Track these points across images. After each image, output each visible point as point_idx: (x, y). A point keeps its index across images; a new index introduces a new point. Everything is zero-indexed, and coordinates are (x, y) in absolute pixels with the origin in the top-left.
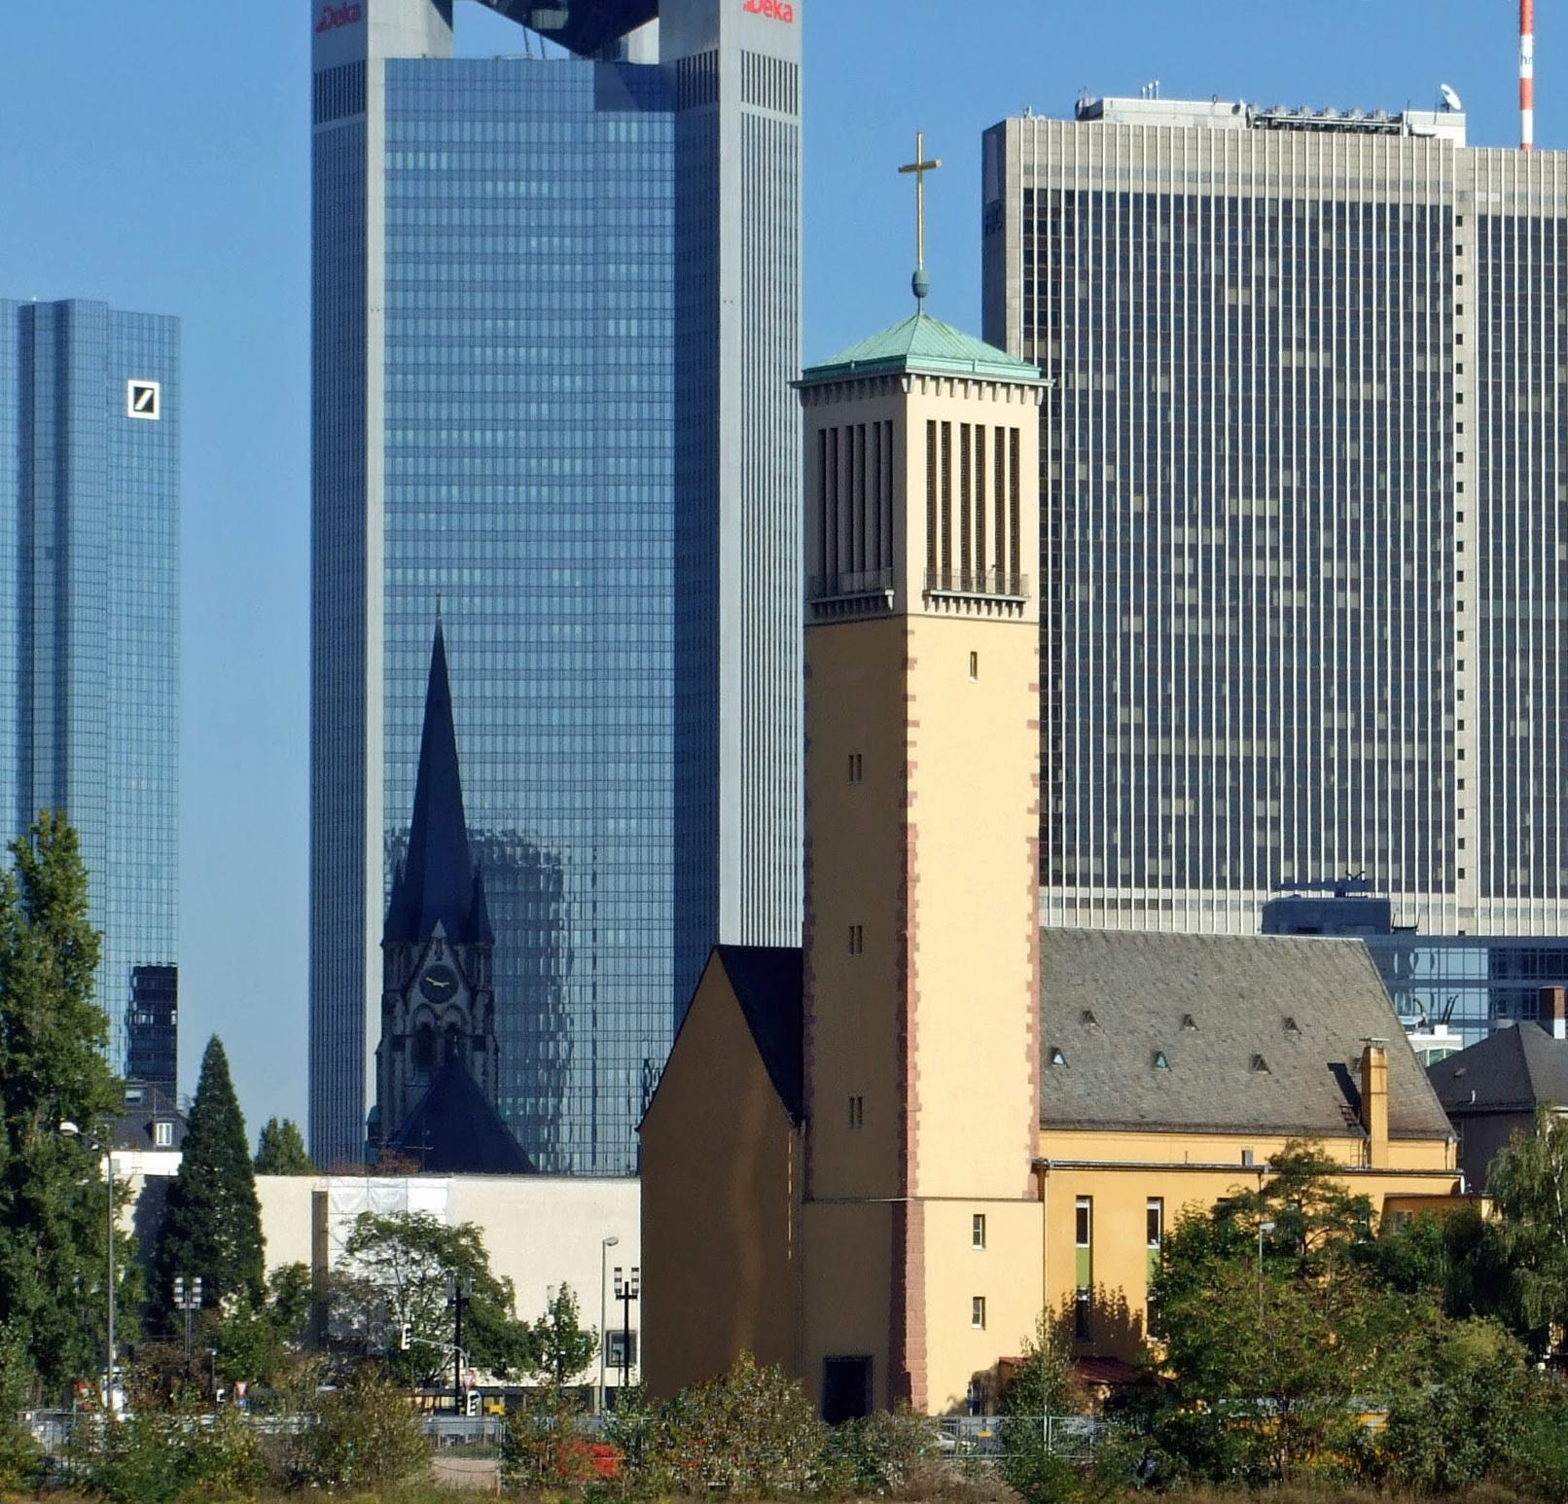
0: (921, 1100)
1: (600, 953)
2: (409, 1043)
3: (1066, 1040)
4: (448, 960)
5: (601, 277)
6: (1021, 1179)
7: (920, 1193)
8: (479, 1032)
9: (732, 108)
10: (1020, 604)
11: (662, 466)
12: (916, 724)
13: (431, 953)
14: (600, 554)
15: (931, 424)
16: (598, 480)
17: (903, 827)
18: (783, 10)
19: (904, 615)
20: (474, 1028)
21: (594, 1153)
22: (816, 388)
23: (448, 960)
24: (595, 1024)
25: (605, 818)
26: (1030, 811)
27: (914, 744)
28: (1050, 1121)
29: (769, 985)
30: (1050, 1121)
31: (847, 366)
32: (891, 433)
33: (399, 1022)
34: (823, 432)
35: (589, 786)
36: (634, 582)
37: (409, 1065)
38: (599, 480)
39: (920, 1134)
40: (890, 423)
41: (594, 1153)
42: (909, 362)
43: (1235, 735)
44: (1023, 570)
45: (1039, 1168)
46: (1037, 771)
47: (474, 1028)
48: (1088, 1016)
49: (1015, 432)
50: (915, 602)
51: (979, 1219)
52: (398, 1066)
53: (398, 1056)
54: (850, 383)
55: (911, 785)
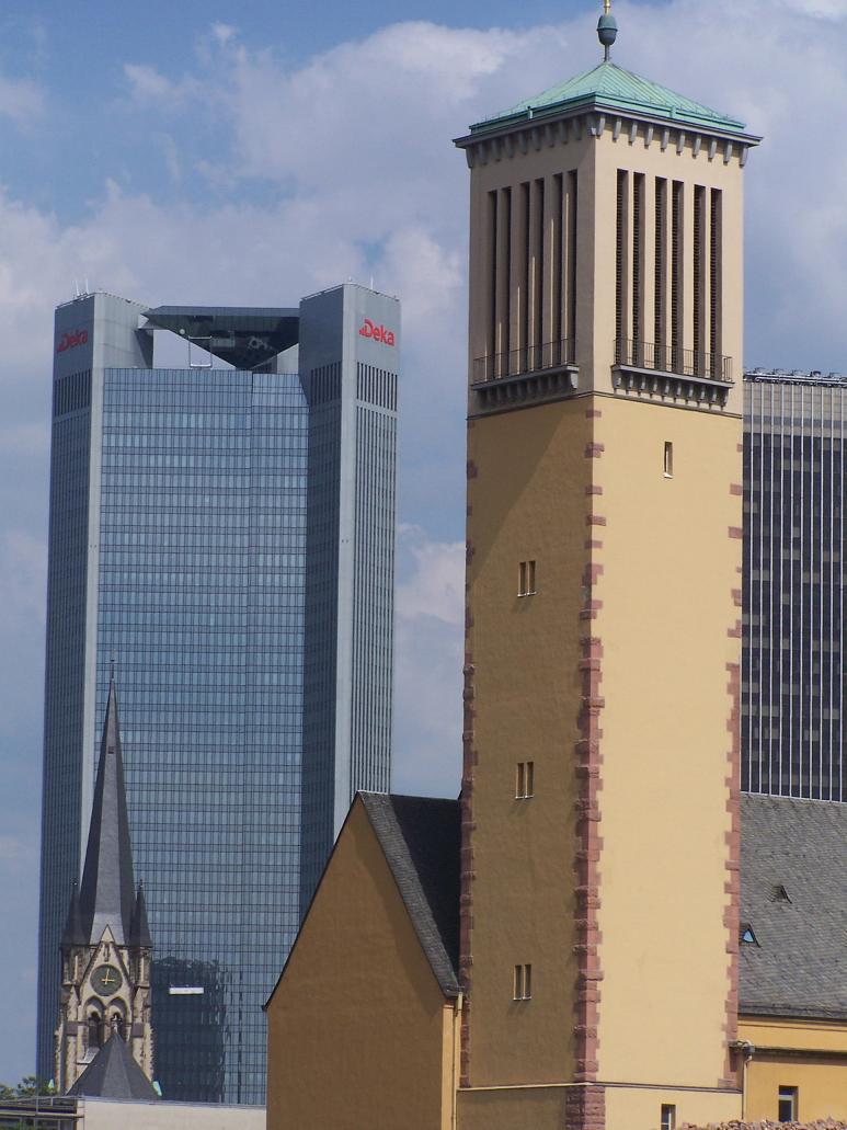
0: (602, 967)
1: (244, 1009)
2: (80, 1029)
3: (756, 916)
4: (114, 961)
5: (252, 642)
6: (715, 1065)
7: (600, 1076)
8: (139, 1020)
9: (349, 403)
10: (723, 392)
11: (295, 679)
12: (602, 522)
13: (100, 955)
14: (250, 722)
15: (622, 174)
16: (252, 550)
17: (587, 644)
18: (387, 337)
19: (591, 394)
20: (134, 1017)
21: (239, 1092)
22: (486, 144)
23: (114, 961)
24: (240, 1060)
25: (258, 514)
26: (731, 634)
27: (599, 545)
28: (748, 1012)
29: (436, 831)
30: (748, 1012)
31: (525, 114)
32: (573, 183)
33: (73, 1010)
34: (493, 195)
35: (240, 829)
36: (275, 682)
37: (80, 1046)
38: (253, 511)
39: (600, 1008)
40: (573, 174)
41: (239, 1092)
42: (597, 99)
43: (806, 771)
44: (725, 352)
45: (738, 1055)
46: (739, 586)
47: (134, 1017)
48: (781, 893)
49: (716, 194)
50: (602, 379)
51: (667, 1110)
52: (71, 1048)
53: (71, 1039)
54: (526, 133)
55: (597, 592)
